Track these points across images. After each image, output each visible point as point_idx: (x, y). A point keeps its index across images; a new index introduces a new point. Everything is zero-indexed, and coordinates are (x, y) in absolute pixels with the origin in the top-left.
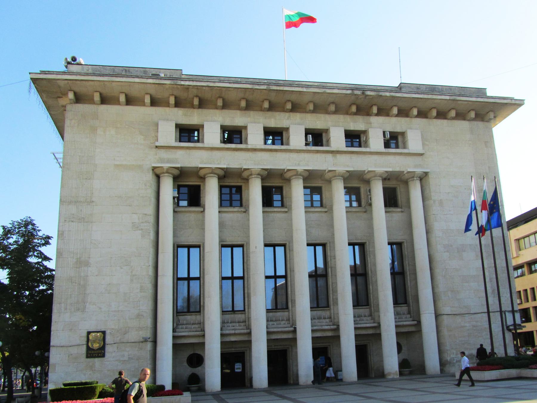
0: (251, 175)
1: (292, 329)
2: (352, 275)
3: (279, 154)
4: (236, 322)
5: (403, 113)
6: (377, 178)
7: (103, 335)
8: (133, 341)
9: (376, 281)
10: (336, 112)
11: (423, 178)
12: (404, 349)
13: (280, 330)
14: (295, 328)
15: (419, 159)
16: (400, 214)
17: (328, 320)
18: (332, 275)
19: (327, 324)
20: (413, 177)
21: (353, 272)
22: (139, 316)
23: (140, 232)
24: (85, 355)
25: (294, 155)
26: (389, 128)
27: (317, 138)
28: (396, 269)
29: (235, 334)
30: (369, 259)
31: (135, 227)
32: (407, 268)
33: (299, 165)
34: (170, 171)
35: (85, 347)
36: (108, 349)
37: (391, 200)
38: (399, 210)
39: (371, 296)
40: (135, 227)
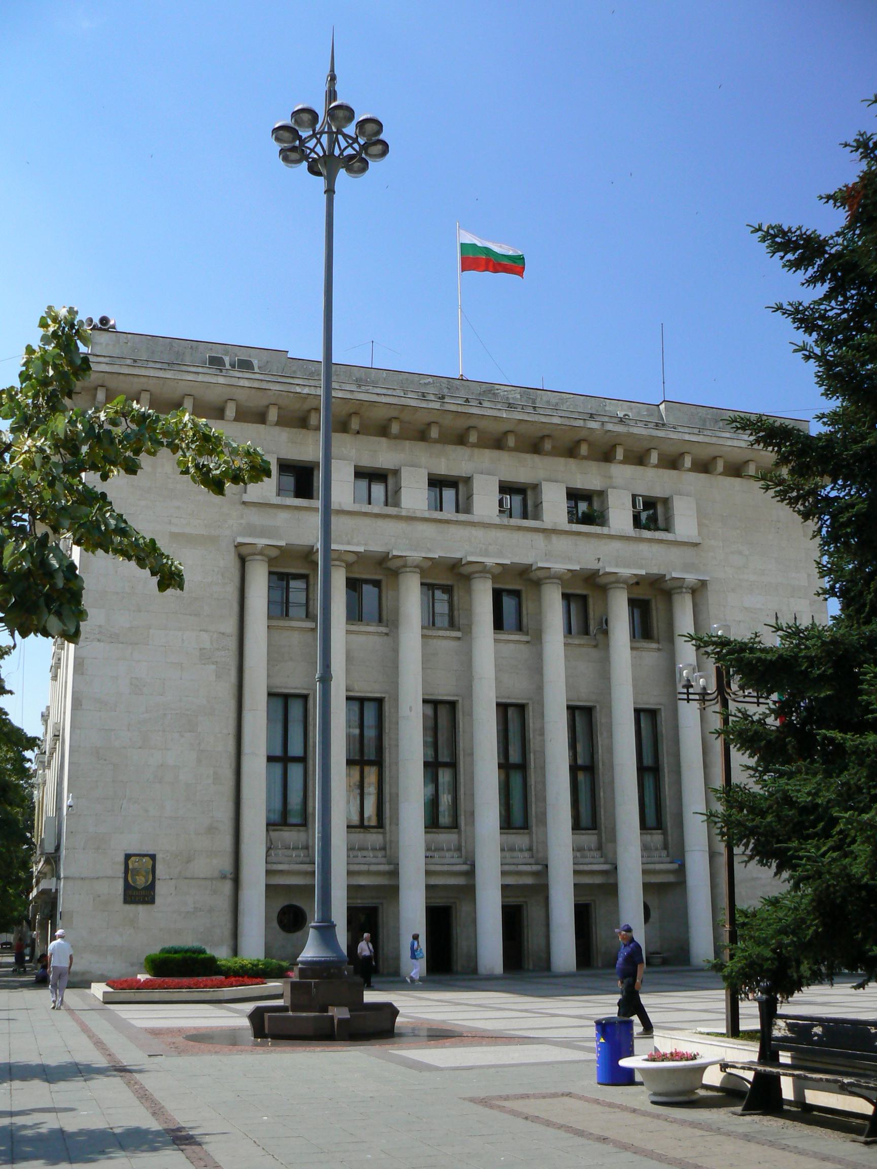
0: (405, 566)
1: (465, 868)
2: (426, 764)
3: (453, 529)
4: (367, 849)
5: (672, 462)
6: (408, 569)
7: (151, 862)
8: (202, 876)
9: (612, 782)
10: (402, 436)
11: (698, 590)
12: (654, 914)
13: (446, 868)
14: (473, 866)
15: (689, 552)
16: (656, 654)
17: (526, 854)
18: (535, 767)
19: (525, 861)
20: (681, 587)
21: (502, 761)
22: (211, 830)
23: (213, 667)
24: (121, 898)
25: (478, 533)
26: (643, 490)
27: (587, 509)
28: (580, 762)
29: (369, 873)
30: (599, 739)
31: (205, 656)
32: (666, 762)
33: (486, 554)
34: (266, 552)
35: (121, 884)
36: (160, 888)
37: (645, 628)
38: (654, 646)
39: (602, 811)
40: (205, 656)
